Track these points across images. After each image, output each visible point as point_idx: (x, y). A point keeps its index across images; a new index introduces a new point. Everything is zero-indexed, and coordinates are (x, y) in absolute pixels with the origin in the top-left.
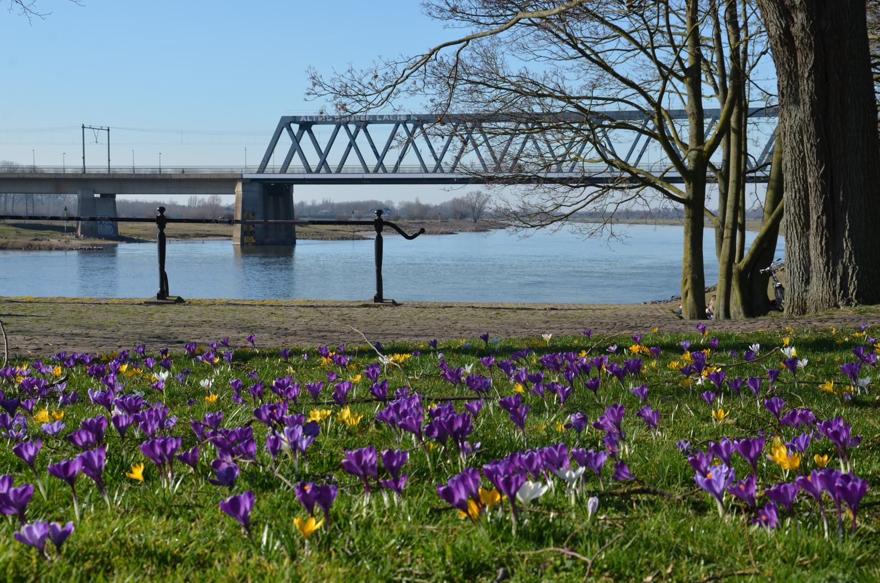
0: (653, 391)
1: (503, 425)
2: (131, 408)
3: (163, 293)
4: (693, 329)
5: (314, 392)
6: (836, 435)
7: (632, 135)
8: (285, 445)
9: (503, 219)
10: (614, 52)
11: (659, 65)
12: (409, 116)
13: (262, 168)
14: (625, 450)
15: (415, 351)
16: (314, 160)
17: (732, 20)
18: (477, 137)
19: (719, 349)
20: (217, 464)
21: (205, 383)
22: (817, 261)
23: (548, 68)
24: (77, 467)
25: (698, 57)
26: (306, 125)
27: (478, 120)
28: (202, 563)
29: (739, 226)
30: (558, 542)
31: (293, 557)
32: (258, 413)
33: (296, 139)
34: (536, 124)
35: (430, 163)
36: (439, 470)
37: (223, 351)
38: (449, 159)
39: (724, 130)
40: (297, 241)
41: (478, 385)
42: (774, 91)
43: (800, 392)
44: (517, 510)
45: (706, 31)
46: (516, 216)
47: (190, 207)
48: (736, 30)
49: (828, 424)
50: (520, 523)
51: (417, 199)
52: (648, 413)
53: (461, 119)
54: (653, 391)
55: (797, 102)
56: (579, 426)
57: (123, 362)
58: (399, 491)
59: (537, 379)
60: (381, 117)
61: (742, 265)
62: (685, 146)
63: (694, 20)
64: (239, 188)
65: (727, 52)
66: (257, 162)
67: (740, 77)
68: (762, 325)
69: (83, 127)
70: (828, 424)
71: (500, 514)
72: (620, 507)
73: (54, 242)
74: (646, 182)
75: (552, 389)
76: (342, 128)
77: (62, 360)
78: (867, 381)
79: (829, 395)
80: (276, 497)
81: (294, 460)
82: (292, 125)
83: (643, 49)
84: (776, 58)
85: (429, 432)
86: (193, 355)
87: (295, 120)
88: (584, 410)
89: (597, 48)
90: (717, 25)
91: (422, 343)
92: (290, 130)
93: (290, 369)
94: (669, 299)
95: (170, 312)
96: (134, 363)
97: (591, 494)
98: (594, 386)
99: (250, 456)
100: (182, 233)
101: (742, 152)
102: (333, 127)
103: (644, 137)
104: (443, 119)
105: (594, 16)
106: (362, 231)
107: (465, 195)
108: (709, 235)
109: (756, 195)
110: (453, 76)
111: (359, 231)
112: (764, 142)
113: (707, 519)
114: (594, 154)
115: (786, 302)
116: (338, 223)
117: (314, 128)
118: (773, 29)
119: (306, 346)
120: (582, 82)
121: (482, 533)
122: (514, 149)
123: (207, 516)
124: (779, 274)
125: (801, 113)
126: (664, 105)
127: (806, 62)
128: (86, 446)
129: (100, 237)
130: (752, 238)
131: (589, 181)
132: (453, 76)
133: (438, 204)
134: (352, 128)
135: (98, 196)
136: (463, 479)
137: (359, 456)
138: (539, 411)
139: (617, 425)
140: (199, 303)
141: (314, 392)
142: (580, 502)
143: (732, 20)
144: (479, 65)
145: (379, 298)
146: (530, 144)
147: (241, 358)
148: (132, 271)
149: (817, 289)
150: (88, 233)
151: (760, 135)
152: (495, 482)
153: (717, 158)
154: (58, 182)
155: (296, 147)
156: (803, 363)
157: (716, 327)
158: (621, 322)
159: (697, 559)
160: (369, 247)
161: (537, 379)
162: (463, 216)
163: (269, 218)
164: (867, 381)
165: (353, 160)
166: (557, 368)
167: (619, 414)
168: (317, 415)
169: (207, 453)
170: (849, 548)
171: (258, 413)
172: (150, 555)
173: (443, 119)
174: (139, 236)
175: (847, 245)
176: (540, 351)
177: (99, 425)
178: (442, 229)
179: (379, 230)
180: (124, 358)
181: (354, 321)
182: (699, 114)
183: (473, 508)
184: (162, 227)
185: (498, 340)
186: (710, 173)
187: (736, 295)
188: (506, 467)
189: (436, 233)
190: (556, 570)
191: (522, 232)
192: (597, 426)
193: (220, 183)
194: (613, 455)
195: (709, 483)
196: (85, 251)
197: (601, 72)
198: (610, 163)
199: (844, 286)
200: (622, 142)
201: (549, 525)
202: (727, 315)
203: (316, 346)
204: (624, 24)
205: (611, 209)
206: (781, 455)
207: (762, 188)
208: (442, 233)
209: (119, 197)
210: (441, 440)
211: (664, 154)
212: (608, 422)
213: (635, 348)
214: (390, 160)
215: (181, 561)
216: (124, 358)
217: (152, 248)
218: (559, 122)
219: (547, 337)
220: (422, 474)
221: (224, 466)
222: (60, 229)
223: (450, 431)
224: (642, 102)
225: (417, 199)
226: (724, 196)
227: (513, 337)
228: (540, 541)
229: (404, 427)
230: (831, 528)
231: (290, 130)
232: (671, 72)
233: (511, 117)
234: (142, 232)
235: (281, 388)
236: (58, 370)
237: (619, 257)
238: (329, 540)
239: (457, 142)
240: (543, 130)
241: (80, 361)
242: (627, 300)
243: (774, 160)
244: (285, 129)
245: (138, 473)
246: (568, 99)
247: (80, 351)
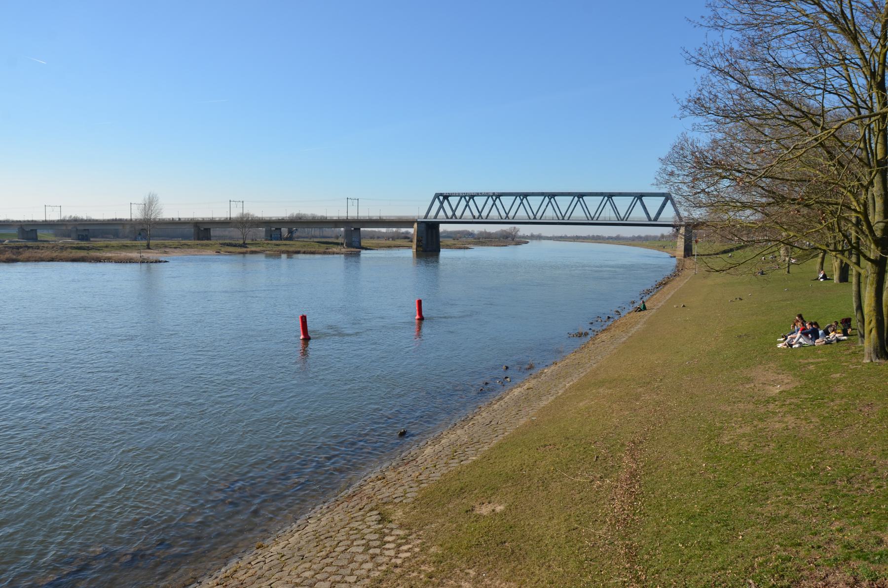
13: (426, 217)
26: (446, 197)
33: (442, 203)
35: (476, 214)
64: (416, 225)
73: (335, 250)
87: (441, 194)
117: (450, 198)
150: (349, 245)
155: (441, 207)
165: (467, 213)
193: (408, 223)
196: (348, 255)
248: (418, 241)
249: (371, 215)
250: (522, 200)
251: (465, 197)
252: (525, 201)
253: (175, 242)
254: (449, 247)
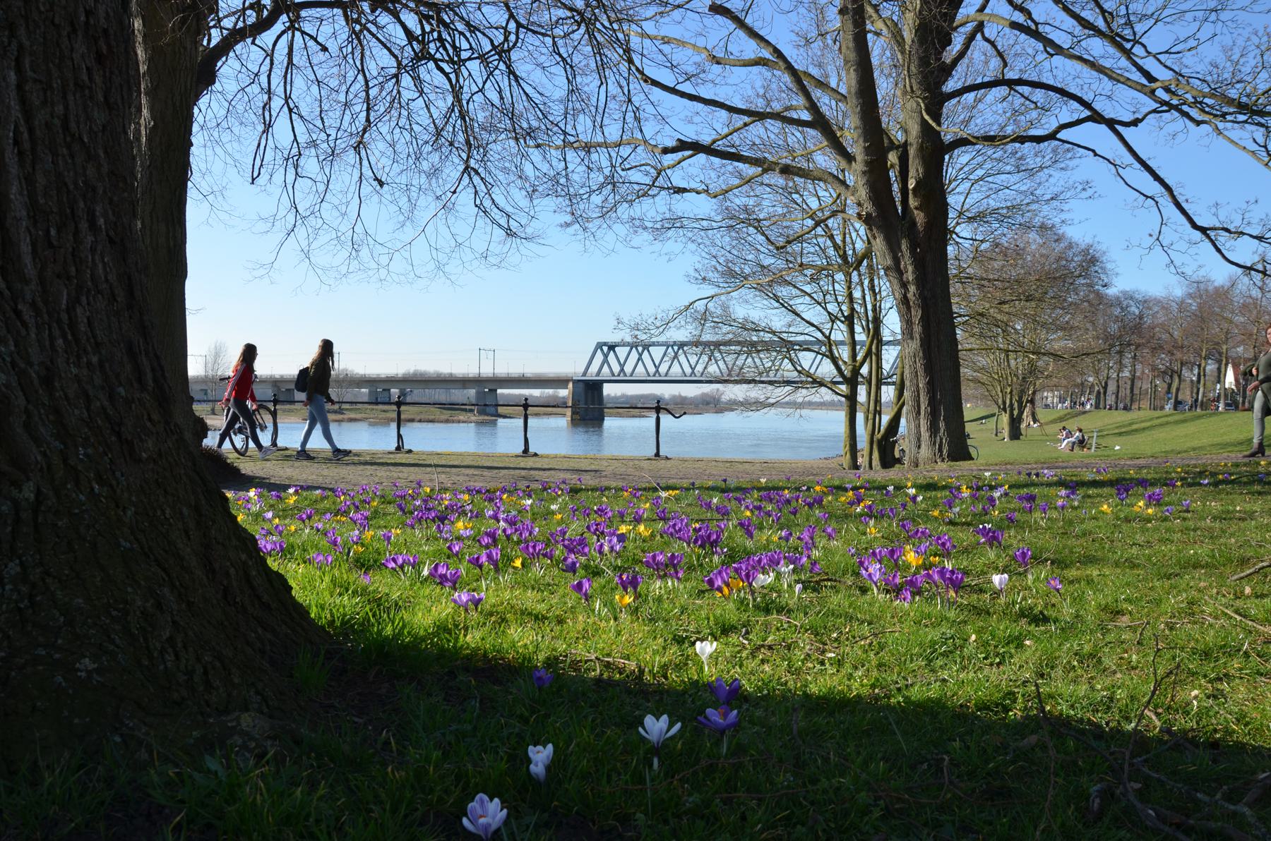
0: (830, 516)
1: (740, 539)
2: (511, 522)
3: (526, 451)
4: (852, 476)
5: (622, 515)
6: (943, 545)
7: (812, 355)
8: (606, 548)
9: (732, 406)
10: (801, 304)
11: (829, 313)
13: (585, 374)
14: (816, 554)
15: (681, 488)
16: (616, 369)
17: (872, 288)
18: (717, 355)
19: (869, 489)
20: (565, 559)
21: (554, 507)
22: (925, 435)
23: (762, 314)
24: (484, 559)
25: (853, 309)
26: (612, 347)
27: (717, 345)
28: (560, 621)
29: (878, 412)
30: (779, 612)
31: (616, 619)
32: (588, 528)
33: (606, 356)
34: (753, 348)
36: (701, 565)
37: (562, 486)
38: (699, 368)
39: (869, 353)
41: (724, 512)
42: (898, 330)
43: (918, 516)
44: (753, 593)
45: (857, 294)
46: (742, 404)
48: (875, 294)
49: (939, 538)
50: (754, 600)
52: (829, 530)
53: (707, 344)
54: (830, 516)
55: (912, 338)
56: (787, 539)
57: (503, 493)
58: (678, 579)
59: (759, 508)
61: (879, 436)
62: (845, 363)
63: (849, 288)
64: (571, 385)
65: (869, 307)
66: (582, 370)
67: (877, 321)
68: (893, 473)
70: (939, 538)
71: (742, 594)
72: (814, 590)
73: (461, 418)
74: (821, 384)
75: (769, 514)
77: (469, 490)
78: (957, 509)
79: (936, 518)
80: (602, 581)
81: (611, 557)
83: (819, 304)
84: (899, 312)
85: (696, 542)
86: (545, 489)
87: (605, 344)
88: (789, 528)
89: (791, 303)
90: (863, 291)
91: (685, 483)
93: (604, 499)
95: (530, 462)
96: (510, 493)
97: (797, 582)
98: (794, 513)
99: (585, 554)
101: (879, 367)
103: (820, 357)
104: (696, 344)
105: (790, 284)
106: (646, 413)
108: (860, 417)
109: (888, 393)
110: (703, 318)
112: (892, 361)
113: (868, 597)
114: (790, 366)
115: (906, 460)
116: (632, 407)
118: (897, 295)
119: (613, 484)
120: (782, 323)
121: (731, 606)
122: (739, 363)
123: (561, 591)
124: (901, 441)
125: (915, 345)
126: (832, 337)
127: (917, 314)
128: (487, 547)
129: (487, 415)
130: (885, 419)
131: (788, 383)
132: (703, 318)
134: (640, 349)
136: (720, 573)
137: (654, 557)
138: (761, 528)
139: (812, 538)
140: (547, 457)
141: (622, 515)
142: (790, 586)
143: (872, 288)
144: (719, 311)
145: (657, 454)
146: (750, 360)
147: (574, 491)
148: (506, 438)
149: (925, 452)
150: (481, 413)
151: (890, 356)
152: (740, 575)
153: (864, 370)
154: (465, 382)
155: (605, 361)
156: (920, 498)
157: (865, 475)
158: (808, 471)
159: (863, 622)
160: (652, 421)
161: (759, 508)
162: (708, 403)
163: (588, 403)
164: (957, 509)
165: (640, 369)
166: (771, 500)
167: (812, 530)
168: (623, 529)
169: (559, 552)
170: (952, 614)
171: (588, 528)
172: (530, 614)
173: (696, 344)
175: (942, 425)
176: (759, 489)
177: (494, 533)
179: (658, 412)
180: (504, 490)
181: (642, 469)
182: (854, 343)
183: (726, 590)
184: (526, 410)
185: (732, 483)
186: (860, 379)
187: (876, 455)
188: (743, 563)
190: (778, 629)
191: (746, 414)
192: (799, 538)
193: (560, 382)
194: (809, 557)
195: (870, 575)
196: (480, 424)
197: (794, 317)
198: (799, 372)
199: (940, 450)
200: (806, 359)
201: (773, 602)
202: (871, 467)
203: (620, 484)
204: (808, 289)
205: (800, 400)
206: (911, 557)
207: (891, 389)
209: (499, 391)
210: (703, 546)
211: (833, 367)
212: (806, 536)
213: (818, 488)
214: (663, 369)
215: (547, 618)
216: (504, 490)
217: (521, 422)
218: (767, 347)
219: (763, 480)
220: (691, 568)
221: (570, 560)
222: (465, 410)
223: (709, 542)
224: (819, 336)
226: (869, 393)
228: (767, 611)
229: (680, 538)
230: (942, 602)
232: (836, 317)
233: (739, 343)
235: (601, 511)
236: (466, 497)
237: (804, 430)
238: (637, 609)
239: (705, 358)
240: (758, 351)
241: (479, 492)
242: (808, 457)
243: (898, 371)
245: (518, 563)
246: (774, 333)
247: (478, 485)
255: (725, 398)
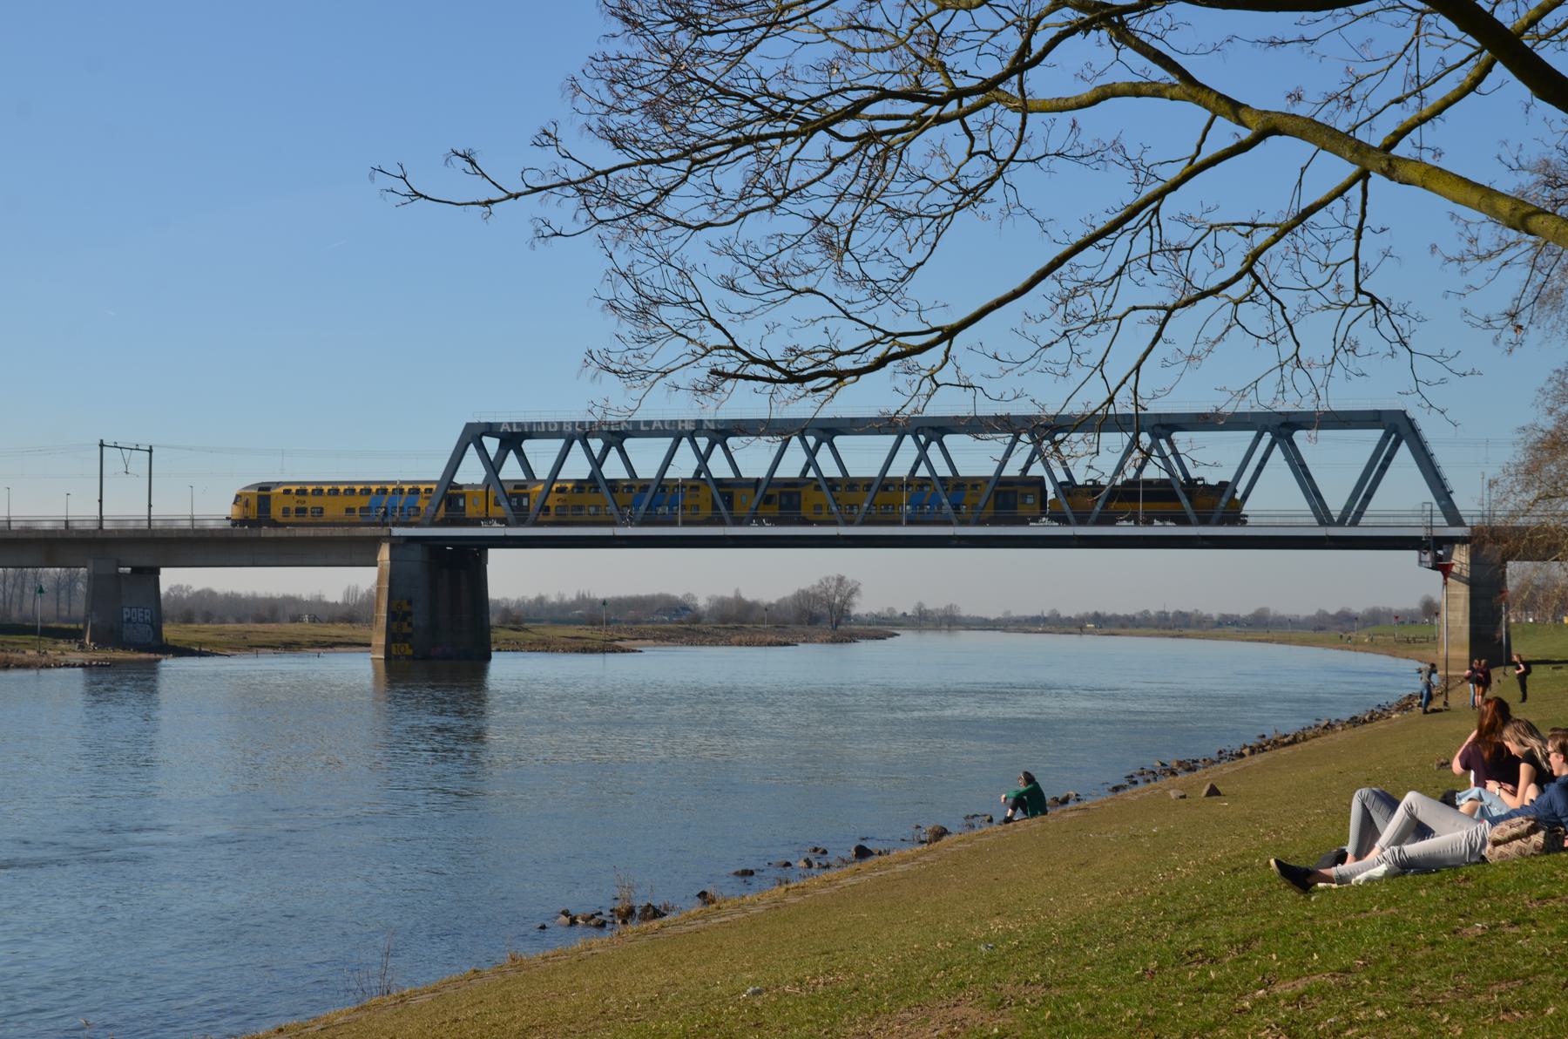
12: (699, 422)
40: (494, 654)
47: (345, 604)
51: (737, 591)
60: (649, 423)
64: (384, 554)
69: (102, 445)
76: (577, 443)
82: (485, 439)
87: (491, 429)
92: (481, 448)
94: (1215, 757)
100: (286, 639)
102: (560, 443)
107: (816, 583)
111: (621, 639)
117: (527, 445)
133: (774, 601)
134: (596, 445)
135: (128, 570)
150: (108, 637)
162: (814, 620)
174: (200, 644)
178: (769, 639)
189: (760, 644)
208: (770, 644)
225: (737, 591)
227: (755, 911)
231: (481, 448)
234: (212, 638)
244: (472, 446)
248: (393, 615)
249: (199, 512)
250: (923, 448)
251: (692, 437)
252: (933, 450)
253: (963, 709)
254: (516, 647)
255: (862, 607)
